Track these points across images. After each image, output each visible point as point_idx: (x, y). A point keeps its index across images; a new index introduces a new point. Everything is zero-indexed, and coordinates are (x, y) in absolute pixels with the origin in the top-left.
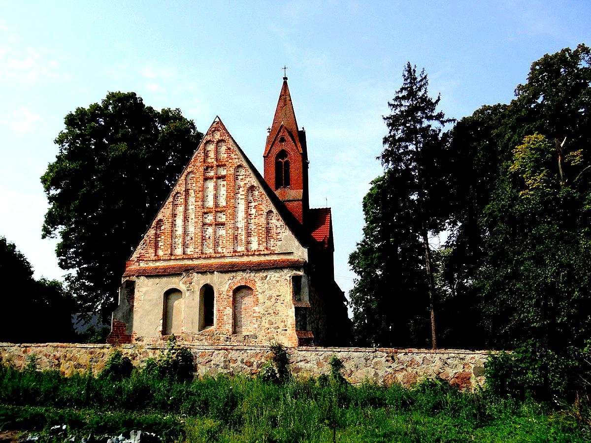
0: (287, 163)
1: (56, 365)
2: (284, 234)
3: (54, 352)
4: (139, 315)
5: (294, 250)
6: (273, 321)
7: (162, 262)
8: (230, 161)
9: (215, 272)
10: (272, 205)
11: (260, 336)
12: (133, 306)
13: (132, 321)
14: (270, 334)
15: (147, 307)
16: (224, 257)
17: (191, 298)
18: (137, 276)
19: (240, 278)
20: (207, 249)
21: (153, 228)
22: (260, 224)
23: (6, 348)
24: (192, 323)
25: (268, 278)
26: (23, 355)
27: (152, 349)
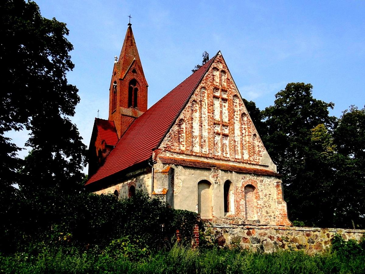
0: (136, 90)
1: (281, 246)
2: (263, 153)
3: (277, 234)
4: (179, 199)
5: (269, 164)
6: (268, 211)
7: (184, 155)
8: (230, 89)
9: (233, 172)
10: (256, 130)
11: (262, 221)
12: (173, 191)
13: (174, 204)
14: (267, 220)
15: (186, 193)
16: (229, 161)
17: (218, 190)
18: (176, 165)
19: (249, 179)
20: (216, 152)
21: (176, 125)
22: (250, 142)
23: (228, 230)
24: (220, 209)
25: (264, 182)
26: (248, 237)
27: (347, 232)
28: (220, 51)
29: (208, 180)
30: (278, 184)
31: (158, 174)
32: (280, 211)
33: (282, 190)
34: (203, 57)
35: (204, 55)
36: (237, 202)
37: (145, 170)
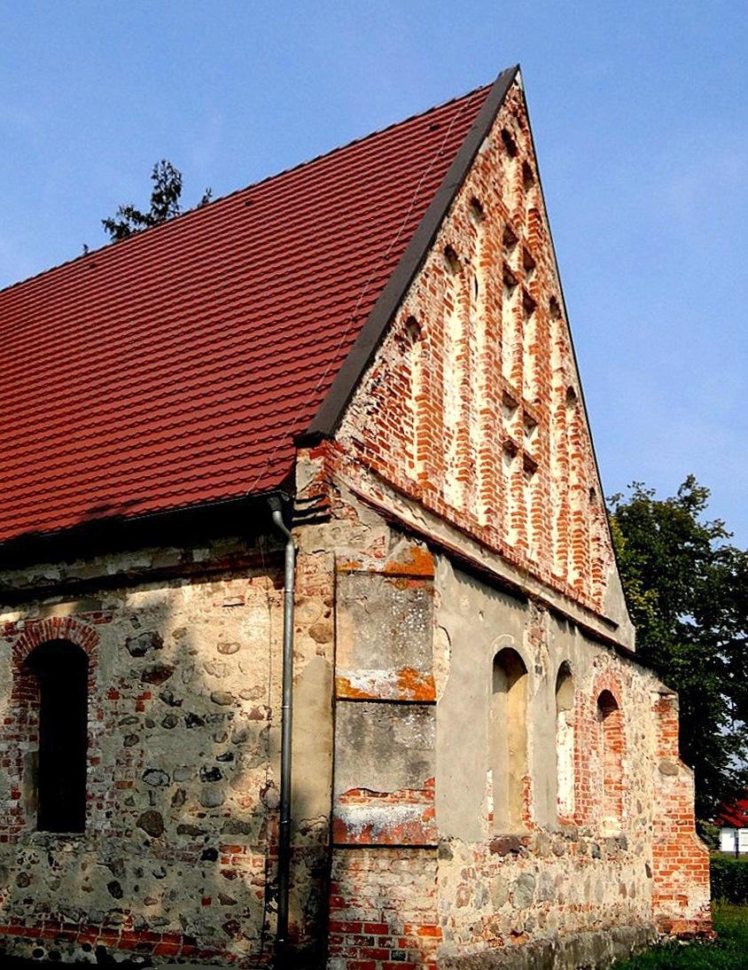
24: (548, 794)
28: (518, 68)
29: (518, 651)
30: (664, 698)
31: (366, 581)
32: (668, 804)
33: (678, 725)
34: (156, 183)
35: (159, 174)
36: (578, 758)
37: (199, 556)
